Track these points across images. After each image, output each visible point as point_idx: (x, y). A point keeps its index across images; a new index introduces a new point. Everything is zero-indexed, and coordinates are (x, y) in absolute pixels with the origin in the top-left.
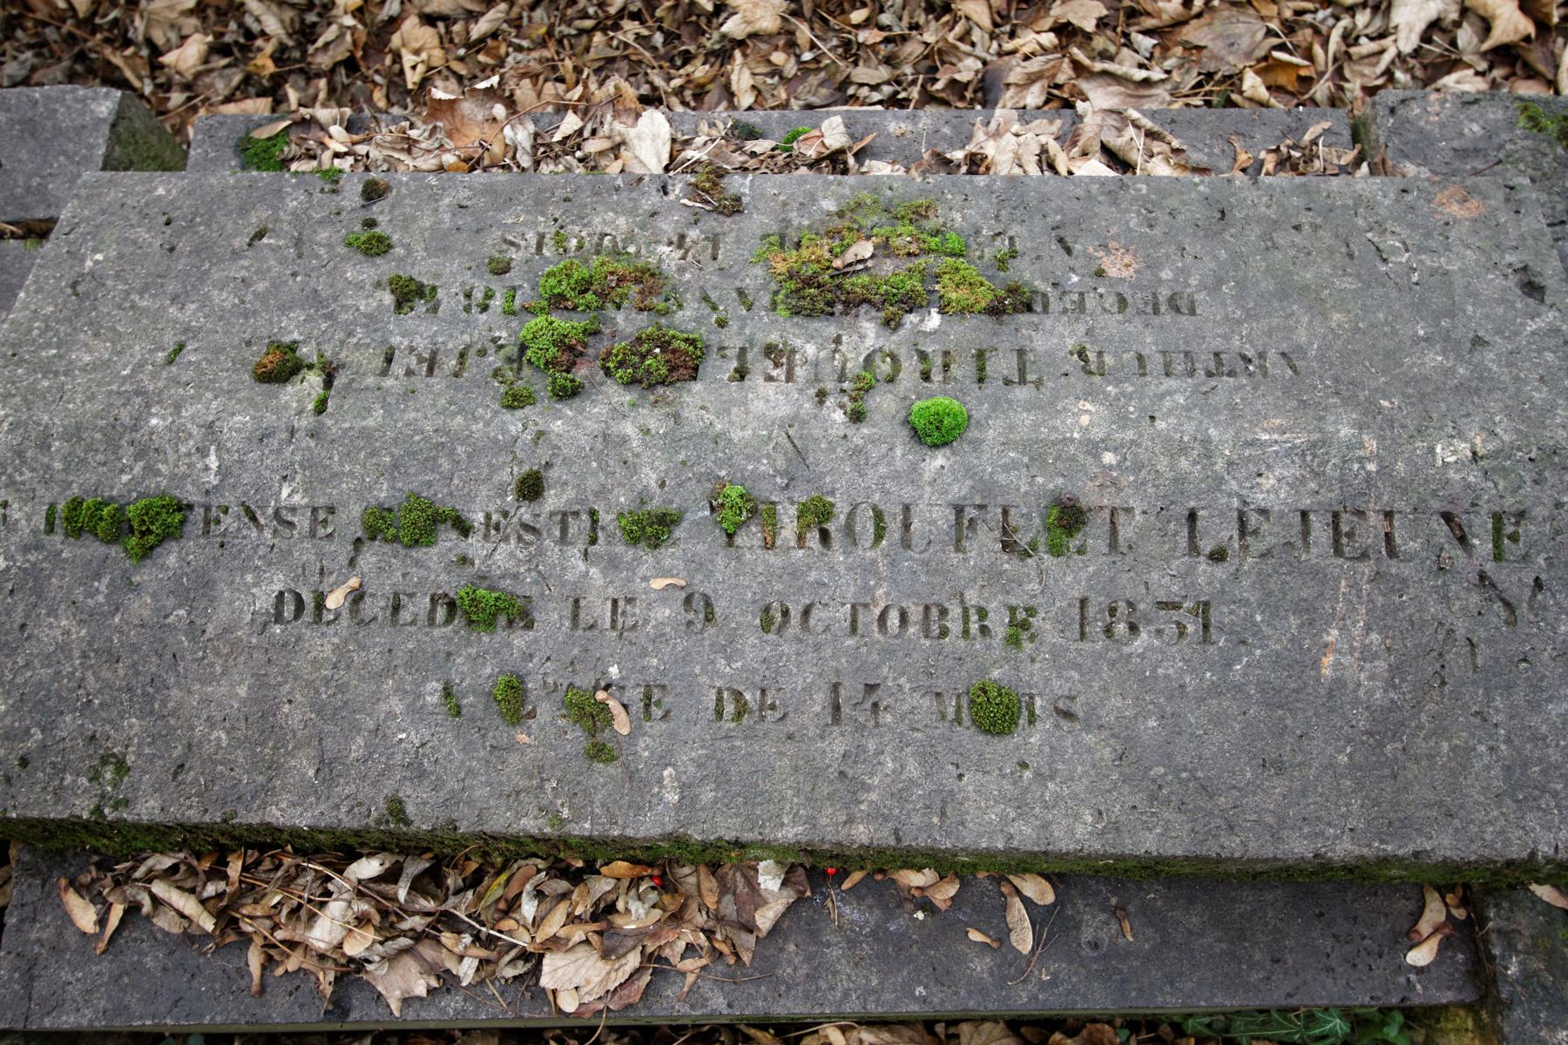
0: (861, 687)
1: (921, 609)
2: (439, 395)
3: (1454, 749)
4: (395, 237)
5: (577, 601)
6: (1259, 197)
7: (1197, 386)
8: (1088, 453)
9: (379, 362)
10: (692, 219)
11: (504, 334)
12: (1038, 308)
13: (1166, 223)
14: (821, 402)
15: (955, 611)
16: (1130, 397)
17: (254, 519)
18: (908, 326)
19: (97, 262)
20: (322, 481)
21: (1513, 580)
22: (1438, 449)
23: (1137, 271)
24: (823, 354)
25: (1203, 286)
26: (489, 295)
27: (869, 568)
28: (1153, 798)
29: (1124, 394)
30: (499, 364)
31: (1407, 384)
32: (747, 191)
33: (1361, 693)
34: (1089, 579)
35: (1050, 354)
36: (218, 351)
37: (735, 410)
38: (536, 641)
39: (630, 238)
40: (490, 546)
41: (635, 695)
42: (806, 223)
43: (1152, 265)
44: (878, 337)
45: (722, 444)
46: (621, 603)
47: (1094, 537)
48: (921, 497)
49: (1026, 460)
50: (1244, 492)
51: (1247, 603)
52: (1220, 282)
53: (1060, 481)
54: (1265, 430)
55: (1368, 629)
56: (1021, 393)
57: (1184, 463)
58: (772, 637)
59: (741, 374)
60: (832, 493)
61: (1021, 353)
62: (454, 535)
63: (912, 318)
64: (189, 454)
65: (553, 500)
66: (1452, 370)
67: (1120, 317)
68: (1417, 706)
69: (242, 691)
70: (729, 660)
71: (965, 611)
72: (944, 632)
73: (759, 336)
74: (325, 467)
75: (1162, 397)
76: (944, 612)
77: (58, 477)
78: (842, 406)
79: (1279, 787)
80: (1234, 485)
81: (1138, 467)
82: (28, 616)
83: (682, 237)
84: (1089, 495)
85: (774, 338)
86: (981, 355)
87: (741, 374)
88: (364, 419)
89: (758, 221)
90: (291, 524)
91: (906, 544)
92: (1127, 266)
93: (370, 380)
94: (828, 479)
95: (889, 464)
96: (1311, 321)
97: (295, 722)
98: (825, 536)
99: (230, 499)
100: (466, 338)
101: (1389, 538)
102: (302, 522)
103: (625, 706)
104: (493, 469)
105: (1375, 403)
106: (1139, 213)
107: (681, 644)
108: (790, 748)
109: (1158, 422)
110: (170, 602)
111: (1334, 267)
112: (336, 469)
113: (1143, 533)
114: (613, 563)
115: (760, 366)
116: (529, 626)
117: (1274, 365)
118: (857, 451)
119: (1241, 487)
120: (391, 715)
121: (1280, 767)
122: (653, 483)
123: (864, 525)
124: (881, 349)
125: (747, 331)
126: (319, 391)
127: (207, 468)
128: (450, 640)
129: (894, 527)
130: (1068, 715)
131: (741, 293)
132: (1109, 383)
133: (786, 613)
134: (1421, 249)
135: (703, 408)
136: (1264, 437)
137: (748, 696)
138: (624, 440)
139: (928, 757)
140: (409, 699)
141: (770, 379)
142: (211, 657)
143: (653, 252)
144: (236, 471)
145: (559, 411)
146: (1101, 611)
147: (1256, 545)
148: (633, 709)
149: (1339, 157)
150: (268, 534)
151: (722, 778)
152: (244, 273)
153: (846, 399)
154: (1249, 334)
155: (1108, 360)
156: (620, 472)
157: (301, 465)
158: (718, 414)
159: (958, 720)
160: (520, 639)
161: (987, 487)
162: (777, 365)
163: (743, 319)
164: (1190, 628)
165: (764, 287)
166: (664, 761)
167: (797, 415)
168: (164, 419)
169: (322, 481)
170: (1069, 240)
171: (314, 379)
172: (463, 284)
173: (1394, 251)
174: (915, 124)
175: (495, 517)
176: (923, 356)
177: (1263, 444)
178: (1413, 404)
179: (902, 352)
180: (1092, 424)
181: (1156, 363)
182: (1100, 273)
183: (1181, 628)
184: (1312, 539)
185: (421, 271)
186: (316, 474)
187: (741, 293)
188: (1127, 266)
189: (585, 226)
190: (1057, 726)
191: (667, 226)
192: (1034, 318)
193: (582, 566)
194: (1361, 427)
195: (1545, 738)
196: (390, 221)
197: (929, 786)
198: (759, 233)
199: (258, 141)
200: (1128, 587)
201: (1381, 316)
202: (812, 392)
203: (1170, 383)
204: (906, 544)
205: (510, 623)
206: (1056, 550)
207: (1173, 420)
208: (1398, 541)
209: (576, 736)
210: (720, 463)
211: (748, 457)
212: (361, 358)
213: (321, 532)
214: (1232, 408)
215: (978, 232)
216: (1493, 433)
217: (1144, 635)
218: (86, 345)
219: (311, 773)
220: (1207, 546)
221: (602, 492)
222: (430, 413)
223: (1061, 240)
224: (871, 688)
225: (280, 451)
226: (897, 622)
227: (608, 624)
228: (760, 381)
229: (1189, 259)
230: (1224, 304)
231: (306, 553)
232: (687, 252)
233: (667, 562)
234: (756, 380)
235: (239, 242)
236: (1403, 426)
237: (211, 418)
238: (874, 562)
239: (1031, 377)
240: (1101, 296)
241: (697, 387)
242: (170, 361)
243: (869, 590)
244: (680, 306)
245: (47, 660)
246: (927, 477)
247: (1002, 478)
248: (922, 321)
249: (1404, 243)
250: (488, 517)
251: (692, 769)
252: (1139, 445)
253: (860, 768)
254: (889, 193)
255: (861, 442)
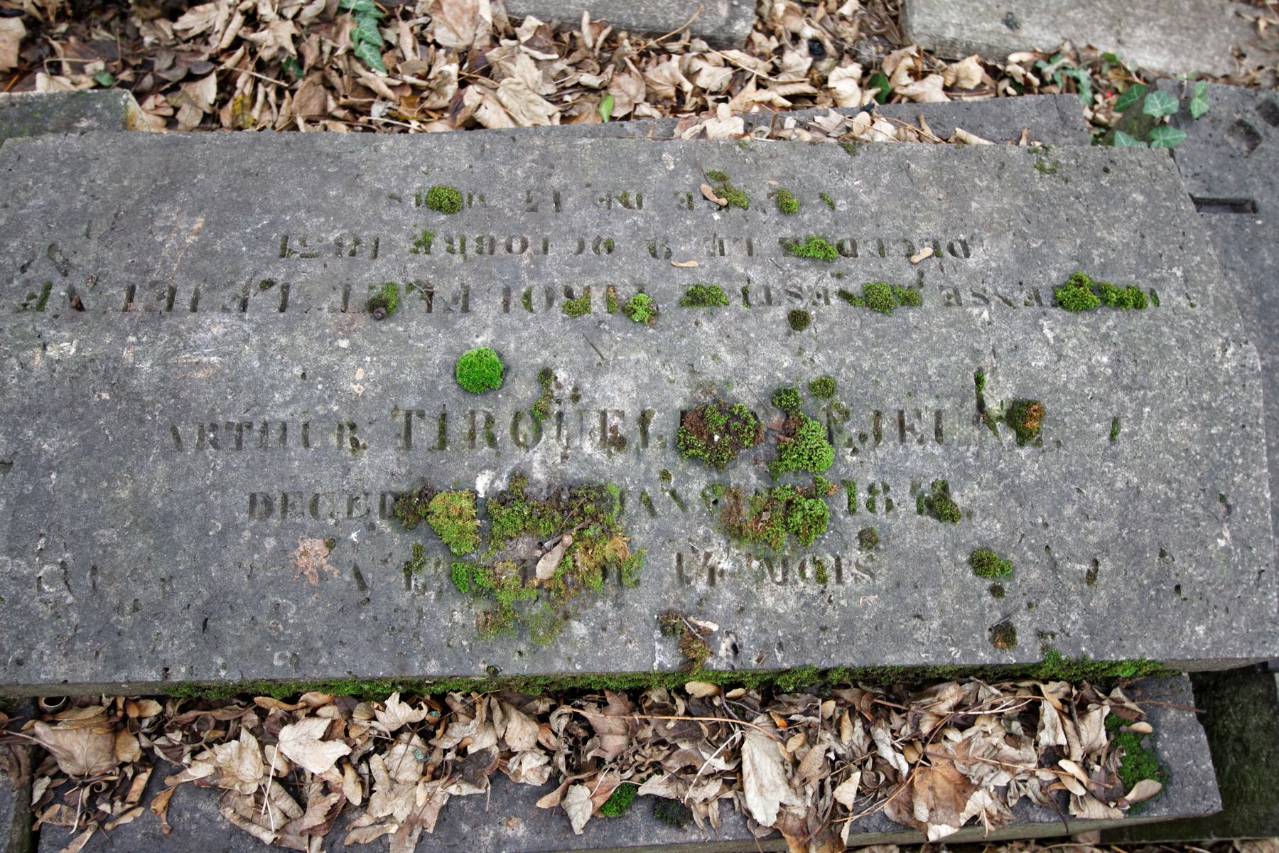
0: (540, 211)
1: (496, 253)
2: (889, 391)
3: (120, 181)
4: (970, 574)
5: (750, 254)
6: (166, 649)
7: (262, 413)
8: (359, 347)
9: (946, 426)
10: (705, 607)
11: (849, 458)
12: (389, 497)
13: (261, 612)
14: (576, 389)
15: (471, 252)
16: (321, 400)
17: (1005, 300)
18: (505, 476)
19: (1221, 536)
20: (960, 322)
21: (42, 271)
22: (73, 350)
23: (297, 546)
24: (577, 442)
25: (238, 529)
26: (871, 506)
27: (534, 274)
28: (339, 157)
29: (325, 402)
30: (847, 424)
31: (82, 417)
32: (658, 646)
33: (178, 209)
34: (369, 269)
35: (383, 446)
36: (1080, 434)
37: (646, 380)
38: (776, 232)
39: (759, 578)
40: (822, 284)
41: (700, 205)
42: (599, 604)
43: (282, 552)
44: (531, 462)
45: (654, 349)
46: (717, 252)
47: (361, 294)
48: (495, 318)
49: (411, 342)
50: (239, 323)
51: (251, 257)
52: (222, 535)
53: (384, 328)
54: (213, 366)
55: (163, 244)
56: (410, 402)
57: (284, 340)
58: (605, 237)
59: (644, 419)
60: (564, 320)
61: (408, 445)
62: (850, 290)
63: (501, 485)
64: (1069, 338)
65: (781, 312)
66: (37, 434)
67: (319, 490)
68: (139, 202)
69: (974, 205)
70: (635, 223)
71: (463, 251)
72: (480, 240)
73: (632, 461)
74: (960, 330)
75: (294, 400)
76: (480, 252)
77: (1162, 323)
78: (559, 386)
79: (249, 163)
80: (246, 327)
81: (321, 339)
82: (1143, 243)
83: (712, 582)
84: (363, 321)
85: (619, 459)
86: (443, 444)
87: (644, 419)
88: (941, 365)
89: (643, 603)
90: (974, 295)
91: (507, 292)
92: (305, 553)
93: (947, 405)
94: (568, 328)
95: (520, 338)
96: (149, 489)
97: (932, 191)
98: (569, 294)
99: (1027, 311)
100: (880, 454)
101: (130, 299)
102: (966, 296)
103: (705, 198)
104: (830, 330)
105: (114, 396)
106: (285, 623)
107: (671, 231)
108: (588, 179)
109: (299, 374)
110: (1045, 251)
111: (113, 555)
112: (952, 330)
113: (324, 296)
114: (728, 275)
115: (627, 428)
116: (781, 241)
117: (191, 437)
118: (546, 346)
119: (241, 327)
120: (868, 193)
121: (246, 173)
122: (705, 324)
123: (538, 300)
124: (527, 448)
125: (642, 466)
126: (985, 393)
127: (1051, 329)
128: (837, 232)
129: (516, 299)
130: (392, 197)
131: (653, 513)
132: (335, 414)
133: (596, 249)
134: (23, 581)
135: (672, 382)
136: (214, 359)
137: (620, 205)
138: (732, 350)
139: (494, 177)
140: (857, 202)
141: (621, 414)
142: (1004, 222)
143: (736, 561)
144: (1029, 329)
145: (788, 377)
146: (361, 252)
147: (238, 289)
148: (700, 197)
149: (60, 813)
150: (990, 290)
151: (634, 166)
152: (1090, 525)
153: (556, 393)
154: (207, 471)
155: (333, 440)
156: (731, 330)
157: (980, 333)
158: (660, 376)
159: (470, 197)
160: (787, 232)
161: (445, 324)
162: (614, 429)
163: (648, 481)
164: (296, 243)
165: (632, 521)
166: (673, 174)
167: (595, 376)
168: (1098, 362)
169: (960, 322)
170: (355, 586)
171: (994, 406)
172: (896, 516)
173: (51, 579)
174: (497, 835)
175: (822, 301)
176: (492, 440)
177: (216, 353)
178: (83, 396)
179: (509, 445)
180: (354, 370)
181: (294, 434)
182: (331, 544)
183: (303, 243)
184: (192, 295)
185: (936, 533)
186: (967, 326)
187: (653, 513)
188: (305, 553)
189: (802, 594)
190: (402, 192)
191: (727, 597)
192: (394, 487)
193: (751, 274)
194: (132, 371)
195: (53, 187)
196: (980, 596)
197: (492, 163)
198: (641, 589)
199: (1152, 777)
200: (339, 265)
201: (85, 496)
202: (584, 401)
203: (283, 415)
204: (507, 292)
205: (797, 242)
206: (392, 287)
207: (287, 375)
208: (124, 295)
209: (738, 184)
210: (653, 337)
211: (631, 340)
212: (958, 429)
213: (951, 292)
214: (236, 390)
215: (440, 593)
216: (22, 365)
217: (331, 239)
218: (1191, 439)
219: (913, 166)
220: (275, 290)
221: (744, 317)
222: (890, 372)
223: (363, 586)
224: (534, 209)
225: (1000, 340)
226: (514, 245)
227: (725, 242)
228: (628, 411)
229: (246, 565)
230: (223, 507)
231: (958, 279)
232: (705, 564)
233: (687, 276)
234: (631, 412)
235: (1106, 565)
236: (96, 372)
237: (1062, 363)
238: (531, 278)
239: (401, 419)
240: (332, 515)
241: (679, 404)
242: (1116, 422)
243: (533, 261)
244: (703, 494)
245: (1116, 219)
246: (490, 330)
247: (430, 329)
248: (492, 482)
249: (40, 589)
250: (827, 302)
251: (655, 169)
252: (318, 352)
253: (540, 169)
254: (523, 647)
255: (543, 352)
